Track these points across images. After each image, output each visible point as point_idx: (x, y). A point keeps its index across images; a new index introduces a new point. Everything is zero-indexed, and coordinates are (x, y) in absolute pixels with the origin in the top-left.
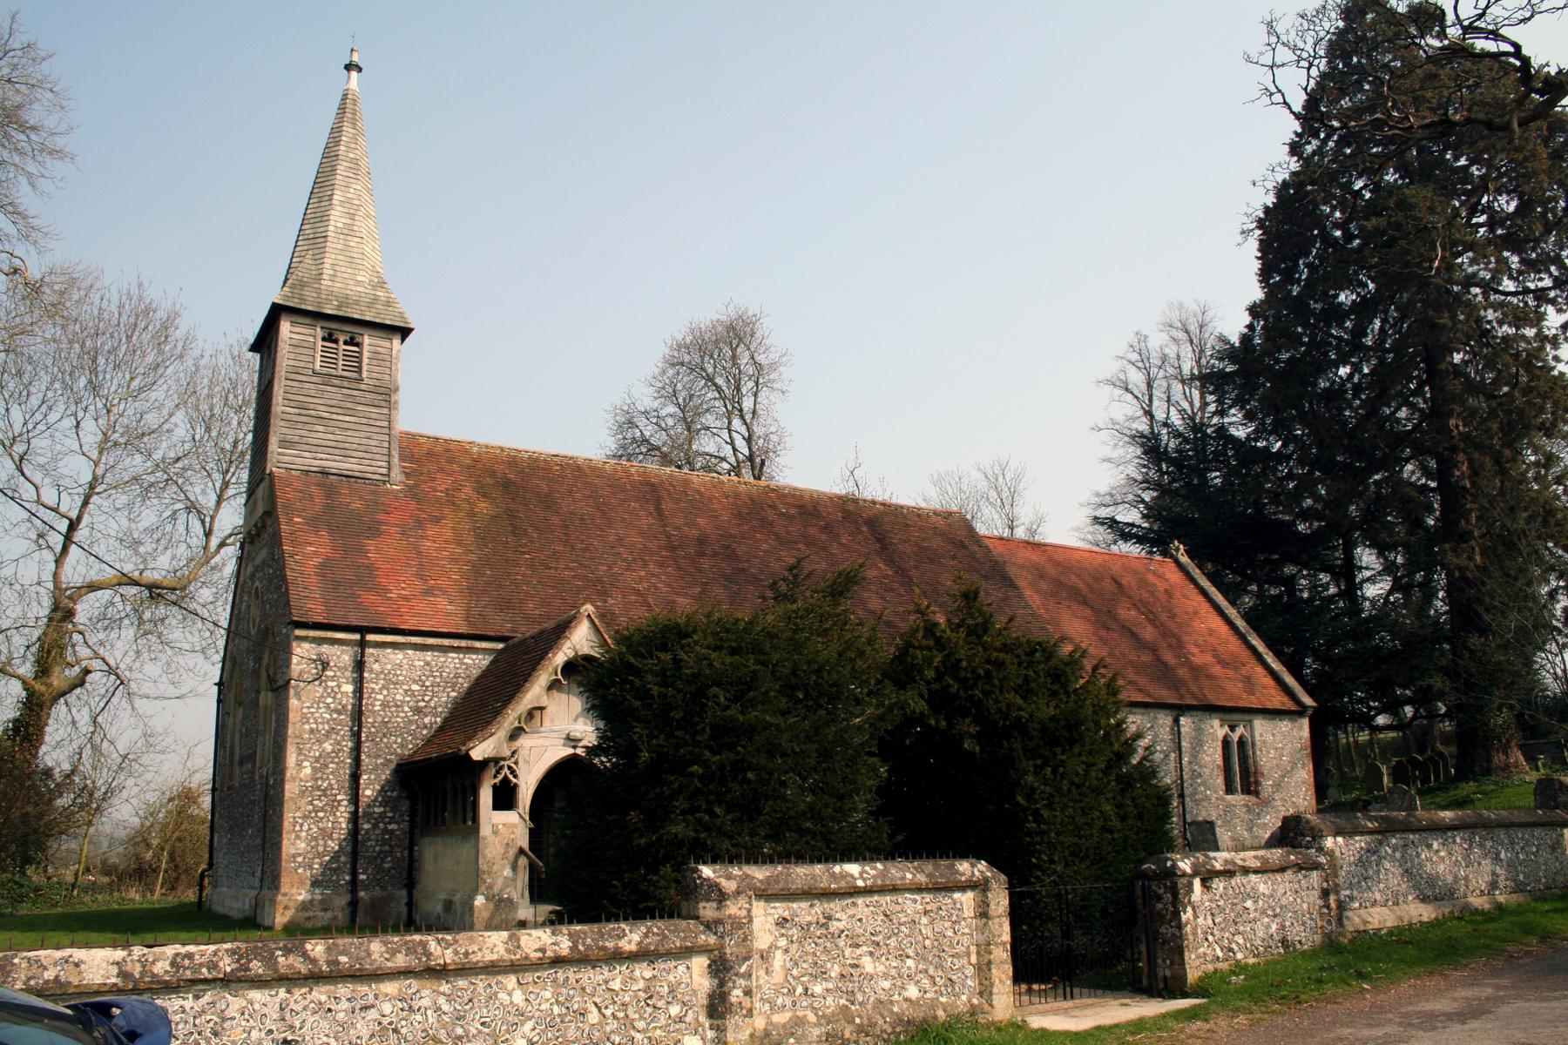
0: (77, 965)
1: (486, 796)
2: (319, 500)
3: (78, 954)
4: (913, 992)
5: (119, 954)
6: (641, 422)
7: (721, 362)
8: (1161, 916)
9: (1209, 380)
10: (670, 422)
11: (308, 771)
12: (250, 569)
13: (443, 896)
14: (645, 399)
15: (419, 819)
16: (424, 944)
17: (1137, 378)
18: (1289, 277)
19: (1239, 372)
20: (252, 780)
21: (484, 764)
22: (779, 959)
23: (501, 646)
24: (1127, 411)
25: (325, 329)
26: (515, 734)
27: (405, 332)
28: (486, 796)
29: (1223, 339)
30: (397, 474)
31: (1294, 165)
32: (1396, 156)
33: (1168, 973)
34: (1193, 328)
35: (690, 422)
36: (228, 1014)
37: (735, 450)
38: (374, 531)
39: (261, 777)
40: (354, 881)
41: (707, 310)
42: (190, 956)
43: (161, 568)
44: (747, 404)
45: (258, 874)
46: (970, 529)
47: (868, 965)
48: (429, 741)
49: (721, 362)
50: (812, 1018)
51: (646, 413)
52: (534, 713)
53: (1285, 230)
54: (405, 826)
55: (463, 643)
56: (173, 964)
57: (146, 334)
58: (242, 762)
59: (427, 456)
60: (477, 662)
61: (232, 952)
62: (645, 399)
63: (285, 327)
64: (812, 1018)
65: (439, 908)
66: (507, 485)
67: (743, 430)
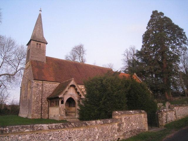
0: (43, 127)
1: (60, 102)
2: (36, 64)
3: (43, 125)
4: (138, 128)
5: (48, 125)
6: (69, 57)
7: (79, 50)
8: (160, 117)
9: (137, 55)
10: (72, 57)
11: (36, 99)
12: (26, 73)
13: (53, 115)
14: (69, 55)
15: (49, 105)
16: (86, 123)
17: (126, 54)
18: (146, 43)
19: (139, 54)
20: (27, 99)
21: (60, 98)
22: (125, 124)
23: (60, 83)
24: (125, 58)
25: (37, 41)
26: (64, 94)
27: (47, 43)
28: (60, 102)
29: (137, 50)
30: (45, 61)
31: (147, 30)
32: (161, 30)
33: (161, 124)
34: (133, 49)
35: (74, 57)
36: (62, 134)
37: (80, 61)
38: (43, 69)
39: (28, 99)
40: (41, 113)
41: (77, 44)
42: (57, 125)
43: (11, 73)
44: (82, 55)
45: (28, 112)
46: (112, 70)
47: (133, 124)
48: (50, 95)
49: (79, 50)
50: (128, 131)
51: (69, 56)
52: (67, 92)
53: (146, 37)
54: (48, 106)
55: (55, 83)
56: (55, 126)
57: (11, 43)
58: (25, 97)
59: (49, 59)
60: (57, 84)
61: (62, 125)
62: (69, 55)
63: (32, 41)
64: (128, 131)
65: (53, 116)
66: (58, 63)
67: (81, 58)
